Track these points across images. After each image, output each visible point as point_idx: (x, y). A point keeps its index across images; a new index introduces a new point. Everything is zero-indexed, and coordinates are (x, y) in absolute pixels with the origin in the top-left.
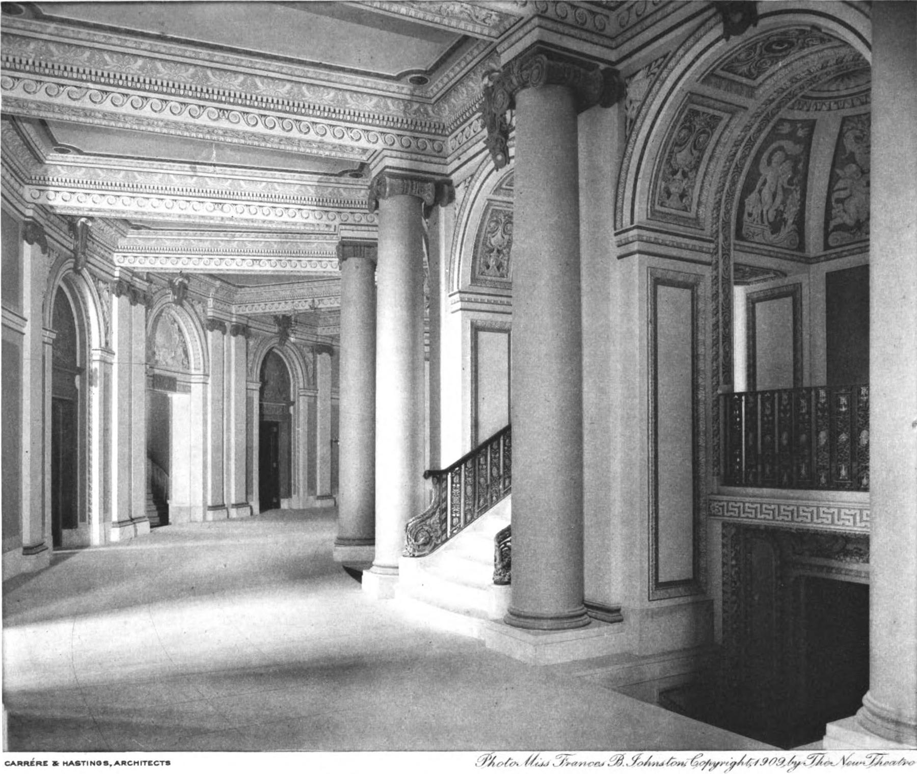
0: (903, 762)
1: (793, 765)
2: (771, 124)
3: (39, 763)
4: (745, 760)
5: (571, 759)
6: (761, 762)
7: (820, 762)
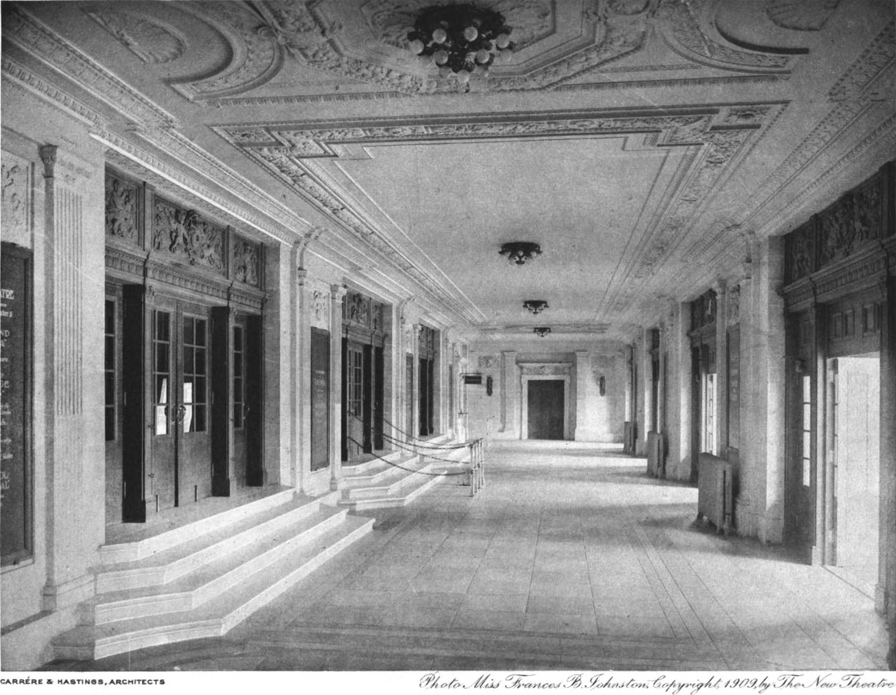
3: (34, 681)
5: (524, 680)
6: (731, 684)
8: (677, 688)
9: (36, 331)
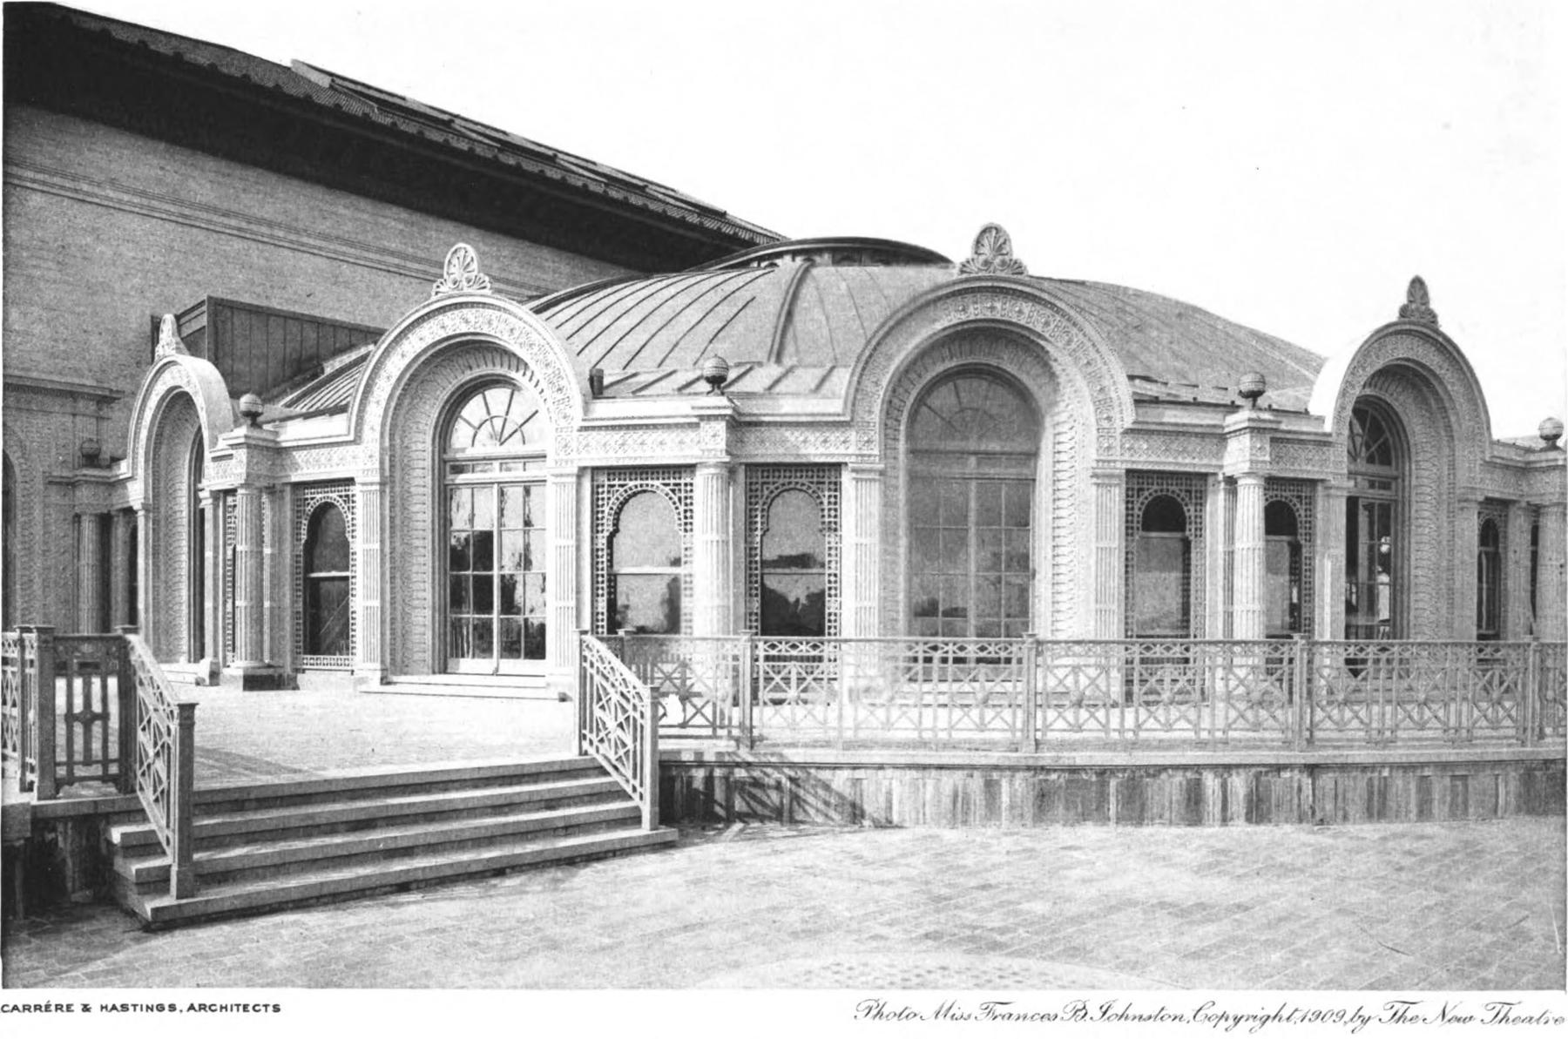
0: (1542, 1019)
3: (59, 1007)
4: (1285, 1013)
7: (1505, 1018)
8: (1231, 1022)
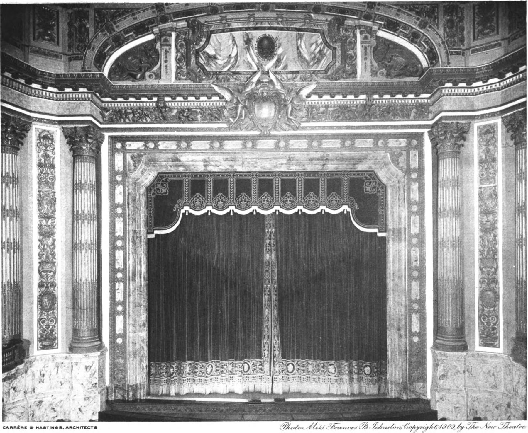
1: (460, 429)
2: (238, 115)
3: (22, 427)
4: (434, 426)
5: (337, 426)
7: (507, 427)
8: (416, 429)
9: (102, 239)
